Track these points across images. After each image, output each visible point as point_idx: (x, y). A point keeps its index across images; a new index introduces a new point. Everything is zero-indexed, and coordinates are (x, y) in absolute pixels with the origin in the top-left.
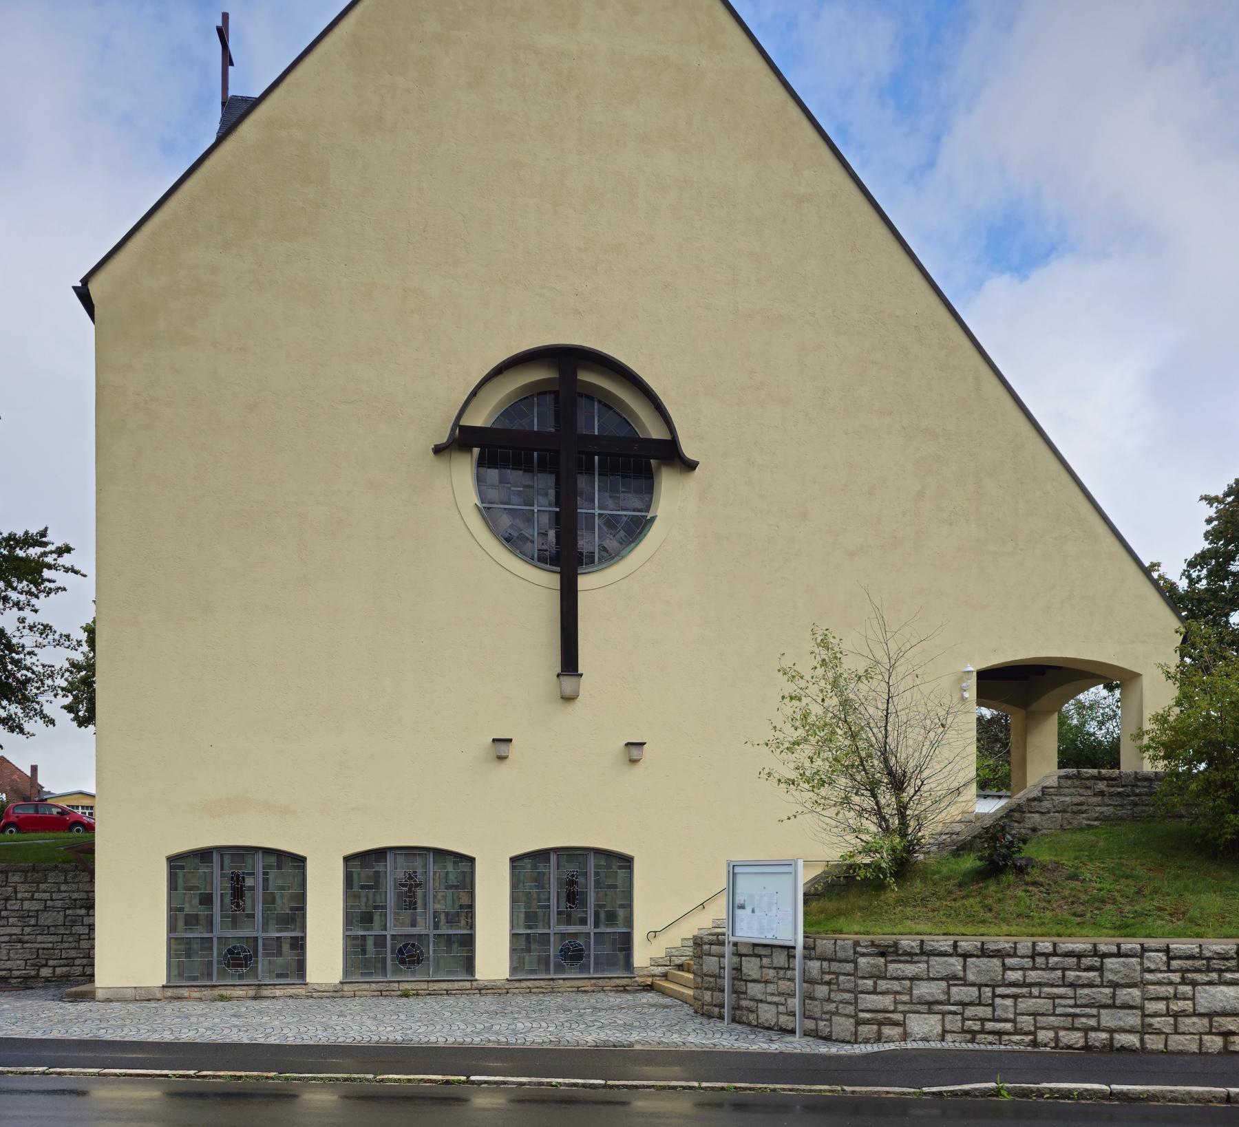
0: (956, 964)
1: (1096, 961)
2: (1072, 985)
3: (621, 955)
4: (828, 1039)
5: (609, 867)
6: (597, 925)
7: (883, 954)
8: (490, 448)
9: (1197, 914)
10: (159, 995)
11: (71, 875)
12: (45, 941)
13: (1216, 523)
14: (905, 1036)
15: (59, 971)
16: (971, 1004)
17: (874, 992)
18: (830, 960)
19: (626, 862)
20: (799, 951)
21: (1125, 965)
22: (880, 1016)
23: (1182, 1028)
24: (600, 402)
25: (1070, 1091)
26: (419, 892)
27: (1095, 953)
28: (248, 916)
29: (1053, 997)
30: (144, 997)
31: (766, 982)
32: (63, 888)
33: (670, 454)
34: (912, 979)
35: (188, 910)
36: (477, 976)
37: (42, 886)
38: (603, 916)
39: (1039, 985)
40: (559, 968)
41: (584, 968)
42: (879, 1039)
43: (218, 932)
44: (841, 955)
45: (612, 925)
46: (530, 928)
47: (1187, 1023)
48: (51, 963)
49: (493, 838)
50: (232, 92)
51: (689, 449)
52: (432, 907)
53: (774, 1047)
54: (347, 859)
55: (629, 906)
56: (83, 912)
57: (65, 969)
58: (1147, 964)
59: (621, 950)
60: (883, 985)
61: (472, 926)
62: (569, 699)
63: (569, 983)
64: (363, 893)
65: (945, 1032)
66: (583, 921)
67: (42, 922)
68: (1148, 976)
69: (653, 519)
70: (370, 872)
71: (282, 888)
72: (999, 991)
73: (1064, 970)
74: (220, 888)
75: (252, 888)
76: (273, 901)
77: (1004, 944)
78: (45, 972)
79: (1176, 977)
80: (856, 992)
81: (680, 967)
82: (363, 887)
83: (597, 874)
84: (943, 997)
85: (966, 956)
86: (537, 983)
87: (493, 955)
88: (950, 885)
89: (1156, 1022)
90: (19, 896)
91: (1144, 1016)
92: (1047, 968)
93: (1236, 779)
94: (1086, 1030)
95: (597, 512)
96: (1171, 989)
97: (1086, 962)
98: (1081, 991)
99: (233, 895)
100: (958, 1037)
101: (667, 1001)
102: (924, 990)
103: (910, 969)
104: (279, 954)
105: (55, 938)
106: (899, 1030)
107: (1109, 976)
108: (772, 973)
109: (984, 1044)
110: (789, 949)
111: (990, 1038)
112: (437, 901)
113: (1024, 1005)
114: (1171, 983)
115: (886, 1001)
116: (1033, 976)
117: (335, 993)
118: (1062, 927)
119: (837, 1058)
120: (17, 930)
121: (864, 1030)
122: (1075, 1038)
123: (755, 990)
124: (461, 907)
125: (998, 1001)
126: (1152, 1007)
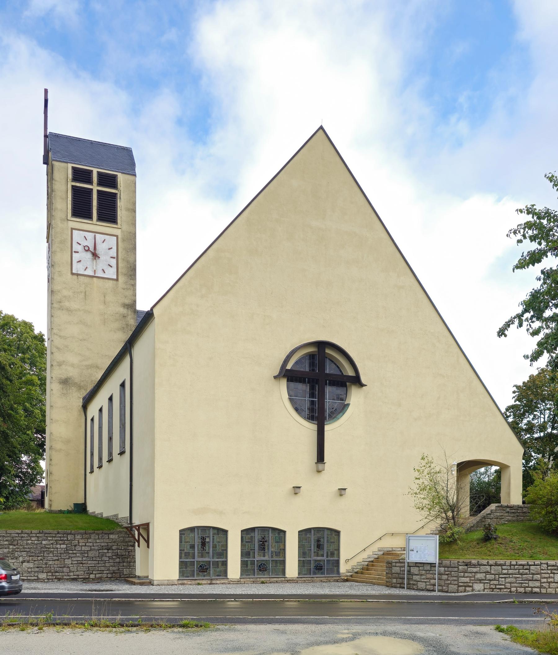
0: (488, 568)
1: (528, 567)
2: (521, 574)
3: (335, 568)
4: (447, 592)
5: (331, 535)
6: (327, 557)
7: (466, 565)
8: (289, 375)
9: (550, 553)
10: (176, 583)
11: (100, 536)
12: (91, 563)
13: (517, 393)
14: (473, 590)
15: (97, 576)
16: (492, 580)
17: (464, 577)
18: (448, 567)
19: (338, 533)
20: (437, 565)
21: (536, 568)
22: (465, 584)
23: (551, 587)
24: (329, 359)
25: (532, 601)
26: (266, 544)
27: (528, 565)
28: (207, 553)
29: (516, 578)
30: (171, 584)
31: (421, 575)
32: (98, 541)
33: (357, 381)
34: (475, 573)
35: (186, 551)
36: (287, 576)
37: (89, 540)
38: (329, 554)
39: (512, 574)
40: (315, 573)
41: (323, 573)
42: (465, 591)
43: (197, 559)
44: (452, 565)
45: (332, 557)
46: (304, 558)
47: (552, 585)
48: (94, 572)
49: (293, 522)
50: (49, 130)
51: (363, 380)
52: (271, 549)
53: (429, 594)
54: (242, 531)
55: (338, 550)
56: (106, 551)
57: (100, 575)
58: (542, 568)
59: (335, 566)
60: (466, 575)
61: (285, 557)
62: (319, 471)
63: (318, 579)
64: (247, 544)
65: (485, 589)
66: (323, 556)
67: (90, 555)
68: (542, 571)
69: (348, 405)
70: (249, 536)
71: (219, 542)
72: (500, 576)
73: (519, 570)
74: (197, 542)
75: (209, 542)
76: (216, 547)
77: (502, 562)
78: (92, 576)
79: (549, 572)
80: (458, 577)
81: (357, 573)
82: (247, 542)
83: (327, 537)
84: (484, 578)
85: (491, 566)
86: (307, 579)
87: (292, 568)
88: (475, 543)
89: (544, 584)
90: (80, 544)
91: (541, 583)
92: (514, 569)
93: (556, 510)
94: (525, 587)
95: (328, 401)
96: (548, 575)
97: (525, 567)
98: (524, 576)
99: (202, 545)
100: (489, 590)
101: (359, 584)
102: (479, 576)
103: (475, 570)
104: (218, 567)
105: (96, 562)
106: (471, 588)
107: (532, 571)
108: (424, 572)
109: (496, 592)
110: (432, 565)
111: (498, 590)
112: (272, 547)
113: (508, 580)
114: (548, 573)
115: (467, 580)
116: (510, 571)
117: (238, 582)
118: (510, 557)
119: (460, 596)
120: (80, 559)
121: (460, 588)
122: (522, 590)
123: (415, 577)
124: (280, 550)
125: (500, 579)
126: (543, 580)
